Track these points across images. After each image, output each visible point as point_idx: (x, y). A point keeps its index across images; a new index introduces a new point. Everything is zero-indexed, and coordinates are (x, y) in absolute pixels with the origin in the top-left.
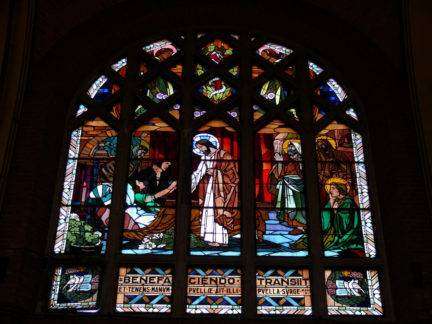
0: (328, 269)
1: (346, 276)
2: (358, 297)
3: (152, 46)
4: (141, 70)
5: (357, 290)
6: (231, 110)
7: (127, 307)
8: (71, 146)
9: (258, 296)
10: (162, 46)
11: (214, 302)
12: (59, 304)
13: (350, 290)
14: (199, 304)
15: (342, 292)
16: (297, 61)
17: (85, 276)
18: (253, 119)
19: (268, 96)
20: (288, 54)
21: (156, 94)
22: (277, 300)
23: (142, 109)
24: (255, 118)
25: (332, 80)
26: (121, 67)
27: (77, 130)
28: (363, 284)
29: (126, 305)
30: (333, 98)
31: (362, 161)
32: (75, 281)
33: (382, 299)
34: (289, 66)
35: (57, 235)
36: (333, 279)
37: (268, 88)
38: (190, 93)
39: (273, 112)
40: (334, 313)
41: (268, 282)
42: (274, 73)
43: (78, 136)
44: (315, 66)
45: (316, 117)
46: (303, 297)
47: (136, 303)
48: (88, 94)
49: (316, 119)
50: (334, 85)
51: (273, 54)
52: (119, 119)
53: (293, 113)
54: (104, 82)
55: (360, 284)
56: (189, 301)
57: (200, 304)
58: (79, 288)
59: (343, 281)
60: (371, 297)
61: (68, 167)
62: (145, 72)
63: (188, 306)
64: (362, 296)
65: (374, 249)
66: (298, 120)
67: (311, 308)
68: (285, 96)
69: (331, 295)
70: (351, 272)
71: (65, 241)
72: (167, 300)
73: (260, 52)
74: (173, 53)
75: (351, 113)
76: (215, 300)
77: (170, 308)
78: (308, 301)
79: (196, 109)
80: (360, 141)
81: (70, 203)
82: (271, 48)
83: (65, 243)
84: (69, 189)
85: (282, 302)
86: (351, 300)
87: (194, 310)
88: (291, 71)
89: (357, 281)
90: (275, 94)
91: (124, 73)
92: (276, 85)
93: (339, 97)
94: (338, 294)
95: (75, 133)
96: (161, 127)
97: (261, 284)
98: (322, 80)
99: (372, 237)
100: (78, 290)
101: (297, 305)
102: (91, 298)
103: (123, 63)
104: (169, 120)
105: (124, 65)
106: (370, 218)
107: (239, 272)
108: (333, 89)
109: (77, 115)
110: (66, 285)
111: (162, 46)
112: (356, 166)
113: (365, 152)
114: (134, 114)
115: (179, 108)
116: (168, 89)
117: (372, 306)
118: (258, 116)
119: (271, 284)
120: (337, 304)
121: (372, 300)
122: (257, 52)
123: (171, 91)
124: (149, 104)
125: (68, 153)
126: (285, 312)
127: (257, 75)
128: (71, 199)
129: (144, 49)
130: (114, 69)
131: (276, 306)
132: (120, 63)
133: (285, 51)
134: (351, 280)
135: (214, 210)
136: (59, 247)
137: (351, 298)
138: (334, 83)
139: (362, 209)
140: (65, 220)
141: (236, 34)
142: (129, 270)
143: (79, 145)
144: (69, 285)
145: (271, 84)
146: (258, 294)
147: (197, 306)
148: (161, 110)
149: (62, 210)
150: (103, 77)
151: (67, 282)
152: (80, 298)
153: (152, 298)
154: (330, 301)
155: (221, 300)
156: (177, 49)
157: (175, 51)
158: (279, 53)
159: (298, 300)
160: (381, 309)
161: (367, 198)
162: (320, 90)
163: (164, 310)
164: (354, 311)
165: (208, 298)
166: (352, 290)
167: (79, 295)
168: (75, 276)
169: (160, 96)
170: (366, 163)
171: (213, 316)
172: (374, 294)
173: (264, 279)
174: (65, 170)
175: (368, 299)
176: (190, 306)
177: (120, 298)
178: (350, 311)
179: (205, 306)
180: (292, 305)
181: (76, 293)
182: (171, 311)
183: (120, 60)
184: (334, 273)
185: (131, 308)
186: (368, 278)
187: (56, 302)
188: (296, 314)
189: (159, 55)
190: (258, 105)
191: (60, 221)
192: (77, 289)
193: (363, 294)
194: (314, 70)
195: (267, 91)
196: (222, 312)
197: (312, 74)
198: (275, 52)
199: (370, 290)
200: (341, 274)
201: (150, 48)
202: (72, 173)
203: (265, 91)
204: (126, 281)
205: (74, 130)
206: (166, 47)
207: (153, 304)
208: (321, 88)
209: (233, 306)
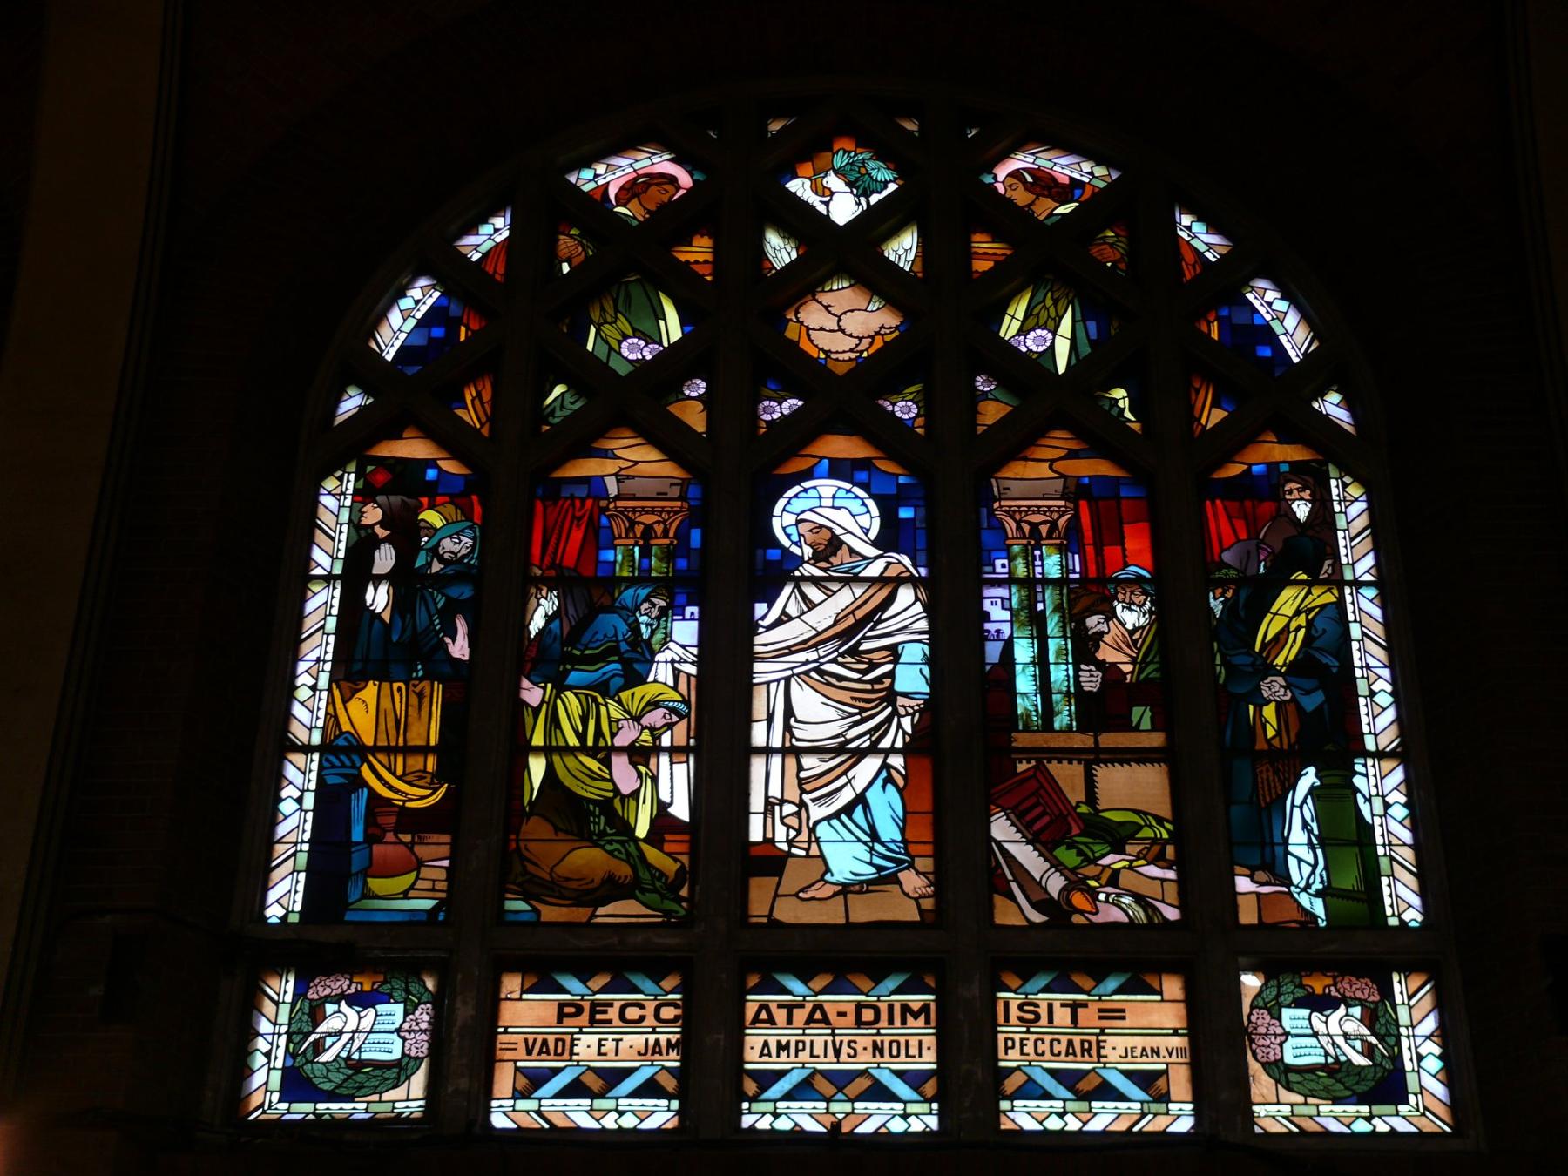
1: (1319, 990)
2: (1363, 1068)
5: (1358, 1044)
6: (895, 390)
8: (318, 532)
9: (1002, 1064)
10: (637, 166)
11: (840, 1090)
12: (286, 1105)
14: (783, 1099)
15: (1302, 1051)
16: (1136, 208)
17: (380, 1008)
19: (1029, 342)
20: (1102, 185)
21: (620, 342)
23: (568, 398)
24: (980, 420)
25: (1261, 283)
26: (489, 244)
27: (339, 473)
28: (1379, 1018)
29: (522, 1104)
30: (1266, 352)
32: (341, 1019)
33: (1450, 1075)
34: (1103, 230)
37: (1027, 315)
38: (744, 328)
39: (1042, 398)
40: (1275, 1128)
42: (1050, 257)
43: (342, 493)
44: (1198, 227)
45: (1203, 421)
47: (558, 1096)
48: (374, 346)
50: (1270, 304)
51: (1043, 183)
52: (485, 431)
53: (1121, 404)
54: (430, 302)
55: (1370, 1019)
56: (750, 1087)
57: (788, 1096)
59: (1306, 1012)
60: (1408, 1066)
61: (310, 606)
62: (576, 261)
63: (745, 1105)
64: (1375, 1065)
65: (1415, 900)
66: (1136, 427)
67: (1190, 1106)
68: (1091, 343)
69: (1263, 1065)
70: (1334, 978)
73: (1001, 177)
74: (678, 188)
75: (1332, 405)
76: (840, 1081)
78: (1180, 1082)
80: (1361, 506)
82: (1039, 162)
84: (314, 688)
85: (1084, 1086)
86: (1339, 1081)
87: (614, 1115)
88: (1111, 245)
89: (1356, 1011)
90: (1054, 334)
91: (501, 270)
93: (1288, 346)
95: (330, 484)
96: (637, 463)
98: (1224, 284)
100: (356, 1056)
101: (1143, 1096)
103: (496, 230)
105: (499, 239)
106: (1403, 788)
107: (931, 982)
108: (1268, 317)
109: (339, 420)
110: (312, 1038)
111: (637, 166)
113: (1376, 549)
114: (541, 415)
115: (702, 391)
116: (662, 323)
117: (1412, 1099)
118: (991, 413)
120: (1286, 1096)
121: (1411, 1080)
122: (988, 179)
123: (673, 328)
124: (591, 376)
126: (1096, 1125)
129: (573, 179)
130: (464, 250)
131: (1065, 1101)
132: (486, 229)
133: (1091, 173)
134: (1336, 1008)
136: (285, 896)
137: (1339, 1071)
138: (1271, 295)
139: (1350, 584)
141: (909, 117)
145: (1039, 297)
147: (779, 1104)
148: (639, 401)
149: (291, 772)
150: (423, 282)
151: (316, 1025)
153: (613, 1077)
154: (1262, 1084)
155: (862, 1084)
156: (692, 175)
157: (685, 179)
158: (1067, 181)
159: (1145, 1080)
160: (1441, 1110)
161: (1390, 714)
162: (1218, 318)
164: (1347, 1121)
165: (818, 1077)
166: (1340, 1041)
167: (363, 1075)
169: (635, 350)
170: (1383, 583)
172: (1420, 1058)
173: (802, 1006)
174: (300, 617)
175: (1399, 1073)
176: (756, 1107)
177: (504, 1080)
178: (1336, 1118)
179: (808, 1105)
180: (1122, 1098)
181: (348, 1067)
183: (486, 222)
184: (1273, 983)
185: (538, 1112)
186: (1398, 999)
187: (276, 1097)
188: (1136, 1129)
189: (629, 201)
190: (992, 374)
193: (1379, 1059)
194: (1195, 243)
195: (1023, 322)
196: (867, 1128)
197: (1189, 257)
198: (1053, 179)
199: (1405, 1042)
200: (1301, 986)
201: (596, 176)
202: (323, 627)
203: (1016, 325)
206: (657, 169)
207: (540, 1099)
208: (1225, 312)
209: (905, 1102)
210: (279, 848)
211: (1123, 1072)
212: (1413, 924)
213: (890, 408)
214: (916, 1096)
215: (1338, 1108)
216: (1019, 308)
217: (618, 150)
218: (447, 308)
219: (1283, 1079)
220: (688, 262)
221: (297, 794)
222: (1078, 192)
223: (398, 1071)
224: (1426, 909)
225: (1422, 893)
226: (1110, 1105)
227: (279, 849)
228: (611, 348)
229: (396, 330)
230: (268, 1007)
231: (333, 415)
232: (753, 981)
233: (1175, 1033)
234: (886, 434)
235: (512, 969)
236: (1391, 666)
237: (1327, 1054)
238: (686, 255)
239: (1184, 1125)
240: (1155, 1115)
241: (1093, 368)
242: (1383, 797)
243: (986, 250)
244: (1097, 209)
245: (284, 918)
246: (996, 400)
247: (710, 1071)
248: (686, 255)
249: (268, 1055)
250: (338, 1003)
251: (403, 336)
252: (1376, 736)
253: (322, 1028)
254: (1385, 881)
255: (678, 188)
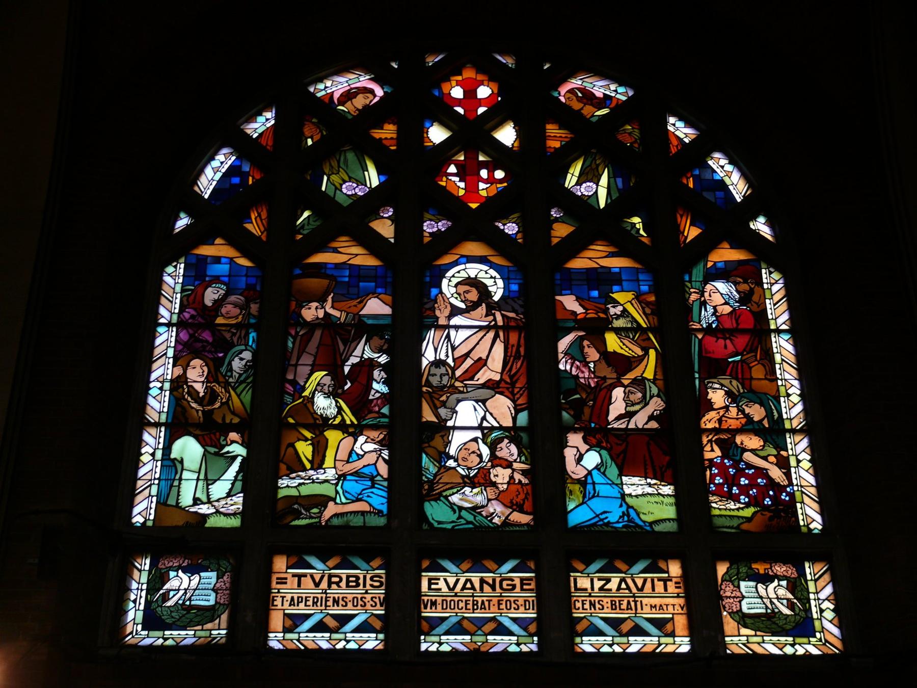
0: (723, 559)
3: (329, 83)
4: (307, 133)
5: (785, 602)
7: (292, 640)
10: (350, 82)
11: (480, 629)
13: (771, 602)
16: (646, 112)
17: (202, 574)
18: (549, 237)
20: (624, 98)
21: (341, 185)
22: (615, 624)
24: (553, 233)
25: (717, 155)
26: (263, 128)
27: (175, 264)
28: (797, 586)
29: (289, 636)
31: (784, 327)
32: (180, 583)
35: (138, 486)
36: (734, 578)
38: (413, 179)
39: (593, 224)
40: (737, 650)
41: (334, 583)
42: (594, 140)
44: (680, 124)
45: (686, 234)
46: (671, 616)
49: (686, 238)
50: (722, 167)
51: (588, 97)
52: (264, 238)
53: (637, 226)
54: (230, 163)
55: (791, 588)
56: (425, 625)
58: (190, 599)
59: (753, 584)
60: (815, 616)
64: (795, 614)
65: (818, 518)
66: (646, 241)
68: (619, 190)
69: (730, 614)
71: (154, 499)
72: (378, 624)
73: (563, 93)
75: (761, 226)
76: (479, 624)
77: (382, 641)
78: (681, 622)
79: (427, 215)
81: (163, 418)
82: (585, 84)
83: (153, 506)
84: (161, 389)
85: (625, 627)
87: (436, 645)
89: (784, 583)
91: (270, 143)
92: (598, 166)
93: (734, 192)
94: (745, 609)
95: (170, 269)
97: (666, 589)
98: (695, 154)
99: (813, 490)
100: (188, 603)
102: (217, 621)
103: (267, 120)
104: (372, 243)
105: (269, 125)
106: (808, 450)
110: (161, 592)
111: (350, 82)
112: (773, 340)
115: (390, 214)
116: (366, 173)
117: (818, 635)
118: (561, 231)
119: (339, 586)
120: (744, 631)
121: (817, 624)
122: (556, 94)
123: (373, 178)
124: (326, 207)
125: (157, 313)
126: (633, 649)
127: (557, 145)
128: (165, 410)
129: (312, 89)
132: (261, 119)
133: (616, 91)
135: (186, 419)
137: (774, 617)
138: (723, 162)
140: (153, 455)
142: (294, 560)
143: (179, 296)
144: (169, 591)
146: (423, 610)
147: (442, 637)
148: (353, 220)
149: (146, 437)
151: (164, 584)
152: (191, 621)
153: (344, 620)
154: (730, 625)
155: (490, 626)
157: (379, 92)
158: (601, 96)
159: (660, 624)
162: (693, 176)
163: (370, 645)
166: (775, 601)
168: (180, 573)
171: (476, 656)
172: (822, 611)
174: (152, 347)
177: (276, 620)
178: (771, 646)
179: (460, 637)
180: (647, 634)
181: (183, 609)
182: (385, 645)
184: (735, 566)
185: (298, 640)
186: (809, 577)
187: (140, 627)
188: (658, 651)
190: (561, 207)
191: (142, 458)
192: (184, 601)
193: (797, 610)
194: (677, 133)
195: (579, 177)
197: (675, 142)
199: (813, 603)
201: (326, 87)
203: (575, 179)
204: (351, 584)
205: (168, 264)
206: (358, 85)
207: (299, 633)
208: (697, 172)
210: (140, 483)
211: (602, 618)
212: (816, 531)
213: (502, 228)
214: (525, 634)
215: (775, 639)
216: (576, 169)
217: (339, 72)
218: (240, 167)
219: (742, 623)
220: (381, 139)
221: (151, 451)
222: (608, 102)
223: (208, 614)
224: (824, 524)
225: (822, 513)
226: (640, 639)
227: (140, 483)
228: (336, 188)
229: (208, 180)
230: (136, 574)
231: (174, 229)
232: (425, 564)
233: (678, 597)
234: (499, 243)
235: (280, 552)
236: (800, 379)
237: (767, 608)
238: (378, 134)
239: (685, 649)
240: (667, 644)
241: (621, 204)
242: (797, 456)
243: (555, 136)
244: (621, 112)
245: (144, 523)
246: (563, 222)
247: (403, 614)
248: (378, 134)
249: (135, 601)
250: (177, 571)
251: (214, 183)
252: (791, 419)
253: (167, 586)
254: (799, 505)
255: (375, 96)
